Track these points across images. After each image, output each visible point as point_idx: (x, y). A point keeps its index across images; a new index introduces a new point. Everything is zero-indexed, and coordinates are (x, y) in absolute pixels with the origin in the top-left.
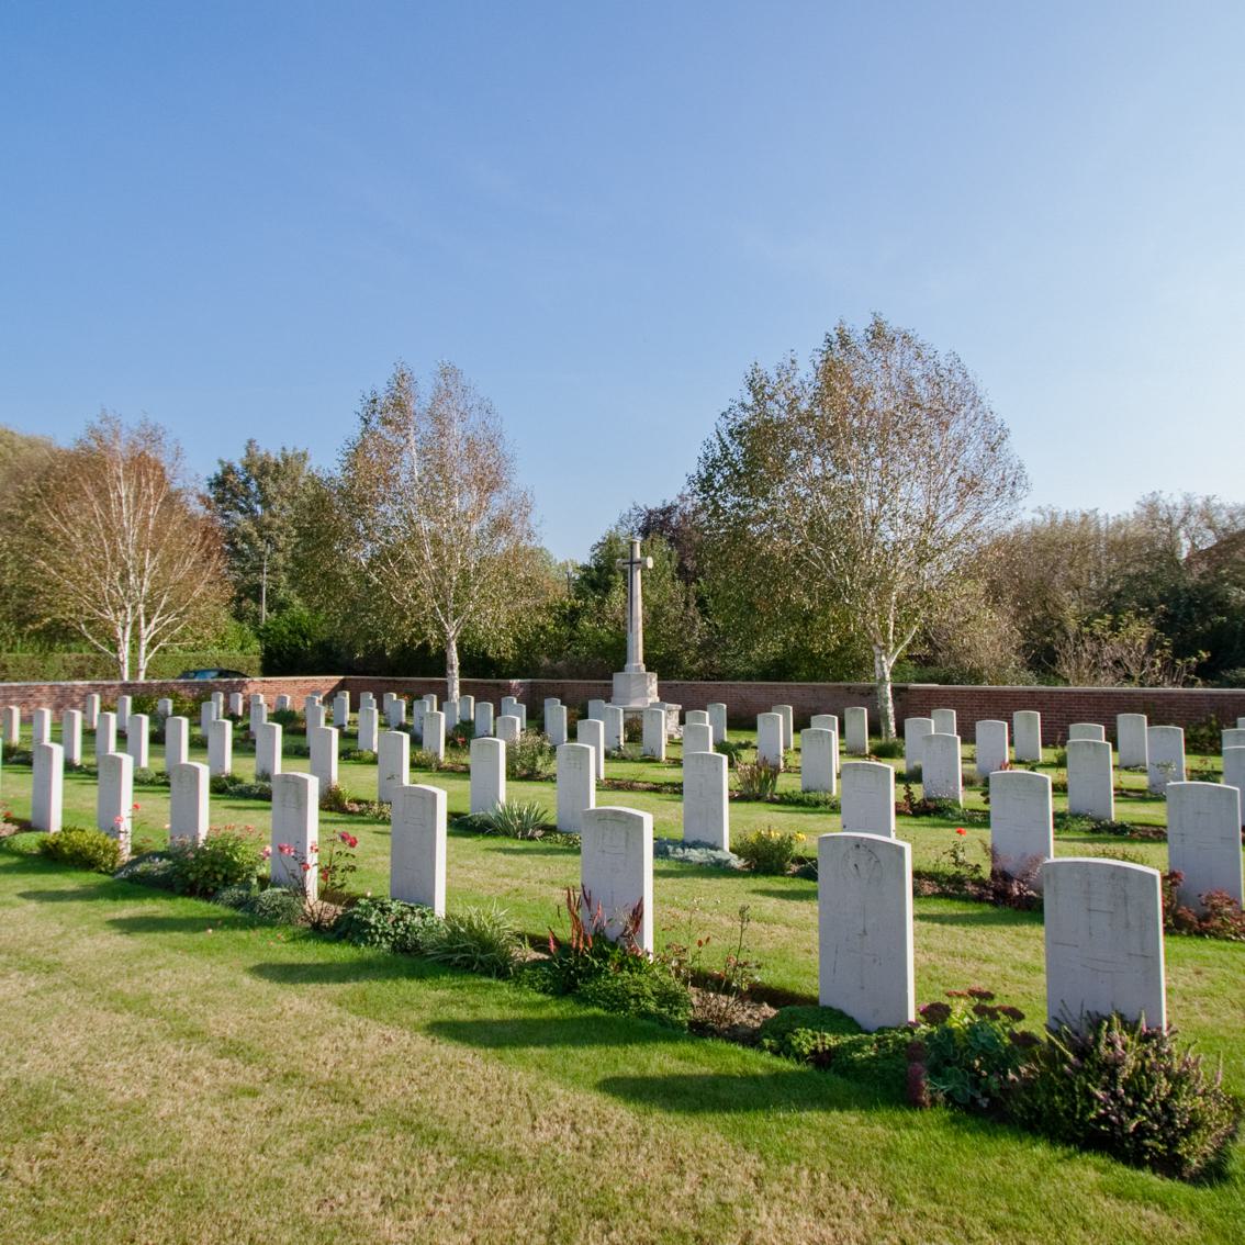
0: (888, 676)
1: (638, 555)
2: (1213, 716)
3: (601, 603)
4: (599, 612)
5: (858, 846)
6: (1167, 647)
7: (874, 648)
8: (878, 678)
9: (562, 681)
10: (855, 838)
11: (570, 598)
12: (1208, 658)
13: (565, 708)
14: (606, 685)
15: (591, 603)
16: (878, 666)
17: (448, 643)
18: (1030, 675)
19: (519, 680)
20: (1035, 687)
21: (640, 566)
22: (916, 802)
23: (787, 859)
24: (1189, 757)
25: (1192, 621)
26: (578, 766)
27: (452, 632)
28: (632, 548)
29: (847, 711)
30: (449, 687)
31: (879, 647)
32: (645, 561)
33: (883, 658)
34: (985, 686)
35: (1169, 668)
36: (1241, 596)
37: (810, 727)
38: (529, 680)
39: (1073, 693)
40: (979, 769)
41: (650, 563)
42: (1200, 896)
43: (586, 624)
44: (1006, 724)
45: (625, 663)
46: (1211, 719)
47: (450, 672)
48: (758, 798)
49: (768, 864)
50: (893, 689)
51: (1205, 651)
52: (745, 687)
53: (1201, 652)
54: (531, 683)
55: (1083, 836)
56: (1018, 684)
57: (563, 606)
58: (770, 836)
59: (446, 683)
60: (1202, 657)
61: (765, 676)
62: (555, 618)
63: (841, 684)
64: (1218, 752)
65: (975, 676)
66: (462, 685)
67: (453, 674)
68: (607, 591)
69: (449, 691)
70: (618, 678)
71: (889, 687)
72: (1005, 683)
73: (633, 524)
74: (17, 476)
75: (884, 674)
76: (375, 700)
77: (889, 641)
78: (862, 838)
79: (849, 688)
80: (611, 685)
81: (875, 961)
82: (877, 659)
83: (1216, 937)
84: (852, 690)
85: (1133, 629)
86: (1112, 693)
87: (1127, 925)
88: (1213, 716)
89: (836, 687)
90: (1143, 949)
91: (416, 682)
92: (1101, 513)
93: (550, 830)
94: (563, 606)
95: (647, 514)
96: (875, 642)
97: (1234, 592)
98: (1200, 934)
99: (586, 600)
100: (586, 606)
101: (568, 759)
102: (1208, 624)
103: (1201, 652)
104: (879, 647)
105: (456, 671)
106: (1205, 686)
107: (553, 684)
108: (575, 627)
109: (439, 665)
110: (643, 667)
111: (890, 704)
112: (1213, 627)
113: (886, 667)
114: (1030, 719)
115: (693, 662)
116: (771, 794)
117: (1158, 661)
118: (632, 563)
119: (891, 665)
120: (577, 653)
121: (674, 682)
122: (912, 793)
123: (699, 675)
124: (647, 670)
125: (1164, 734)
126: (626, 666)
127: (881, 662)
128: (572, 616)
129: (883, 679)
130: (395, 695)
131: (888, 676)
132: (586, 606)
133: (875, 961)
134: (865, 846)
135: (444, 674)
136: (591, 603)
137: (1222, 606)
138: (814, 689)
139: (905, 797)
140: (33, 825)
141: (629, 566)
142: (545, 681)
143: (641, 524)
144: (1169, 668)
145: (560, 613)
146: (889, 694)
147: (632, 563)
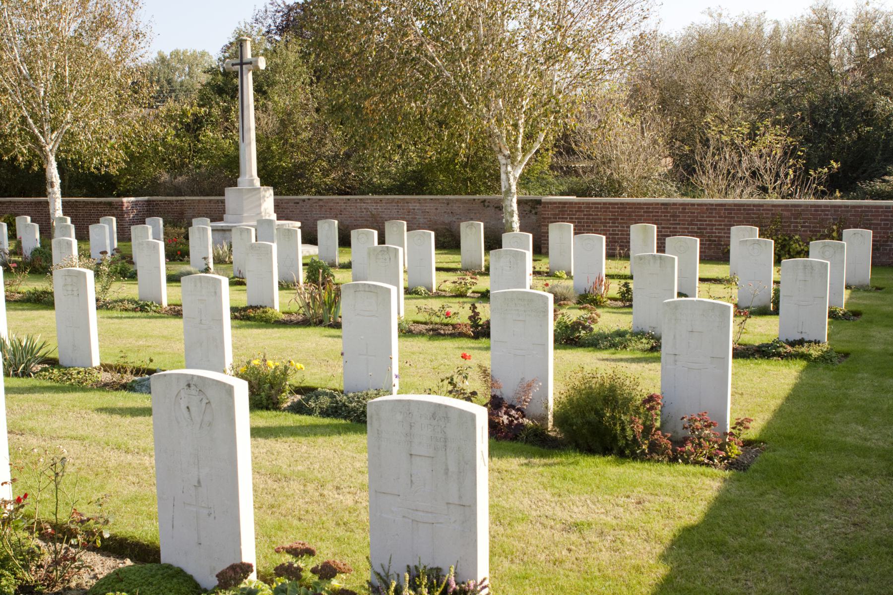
0: (514, 188)
1: (248, 55)
2: (835, 227)
3: (227, 110)
4: (227, 120)
5: (189, 385)
6: (800, 157)
7: (500, 157)
8: (503, 189)
9: (183, 198)
10: (186, 375)
11: (192, 106)
12: (838, 169)
13: (37, 226)
14: (218, 201)
15: (216, 111)
16: (503, 176)
17: (46, 157)
18: (671, 187)
19: (132, 199)
20: (678, 199)
21: (251, 67)
22: (481, 323)
23: (282, 391)
24: (702, 265)
25: (840, 132)
26: (75, 293)
27: (51, 144)
28: (241, 46)
29: (387, 225)
30: (51, 207)
31: (504, 155)
32: (257, 62)
33: (509, 168)
34: (625, 199)
35: (802, 181)
36: (885, 105)
37: (501, 248)
38: (146, 198)
39: (706, 205)
40: (575, 287)
41: (262, 64)
42: (683, 418)
43: (209, 134)
44: (376, 233)
45: (238, 177)
46: (834, 231)
47: (50, 190)
48: (320, 323)
49: (258, 398)
50: (519, 202)
51: (836, 161)
52: (375, 202)
53: (832, 162)
54: (148, 201)
55: (639, 355)
56: (660, 196)
57: (184, 114)
58: (266, 366)
59: (47, 203)
60: (833, 167)
61: (401, 189)
62: (175, 128)
63: (477, 197)
64: (627, 257)
65: (615, 188)
66: (65, 205)
67: (54, 193)
68: (233, 97)
69: (51, 211)
70: (230, 193)
71: (515, 200)
72: (645, 195)
73: (270, 21)
74: (105, 22)
75: (510, 186)
76: (73, 227)
77: (517, 149)
78: (193, 376)
79: (484, 201)
80: (223, 202)
81: (209, 515)
82: (503, 169)
83: (686, 462)
84: (486, 204)
85: (769, 138)
86: (651, 204)
87: (447, 471)
88: (835, 227)
89: (469, 200)
90: (460, 497)
91: (22, 203)
92: (770, 16)
93: (53, 363)
94: (184, 114)
95: (286, 11)
96: (500, 151)
97: (882, 101)
98: (673, 460)
99: (211, 108)
100: (210, 115)
101: (65, 285)
102: (855, 135)
103: (832, 162)
104: (504, 155)
105: (57, 189)
106: (842, 197)
107: (171, 202)
108: (196, 138)
109: (39, 184)
110: (257, 182)
111: (516, 218)
112: (859, 137)
113: (512, 178)
114: (645, 230)
115: (326, 173)
116: (334, 319)
117: (791, 172)
118: (242, 64)
119: (518, 176)
120: (199, 166)
121: (305, 197)
122: (477, 314)
123: (329, 190)
124: (262, 185)
125: (756, 246)
126: (239, 180)
127: (507, 173)
128: (194, 126)
129: (508, 191)
130: (29, 218)
131: (514, 188)
132: (210, 115)
133: (209, 515)
134: (195, 385)
135: (44, 193)
136: (216, 111)
137: (869, 117)
138: (448, 202)
139: (470, 318)
140: (60, 363)
141: (239, 67)
142: (163, 198)
143: (279, 21)
144: (802, 181)
145: (181, 123)
146: (515, 206)
147: (242, 64)
